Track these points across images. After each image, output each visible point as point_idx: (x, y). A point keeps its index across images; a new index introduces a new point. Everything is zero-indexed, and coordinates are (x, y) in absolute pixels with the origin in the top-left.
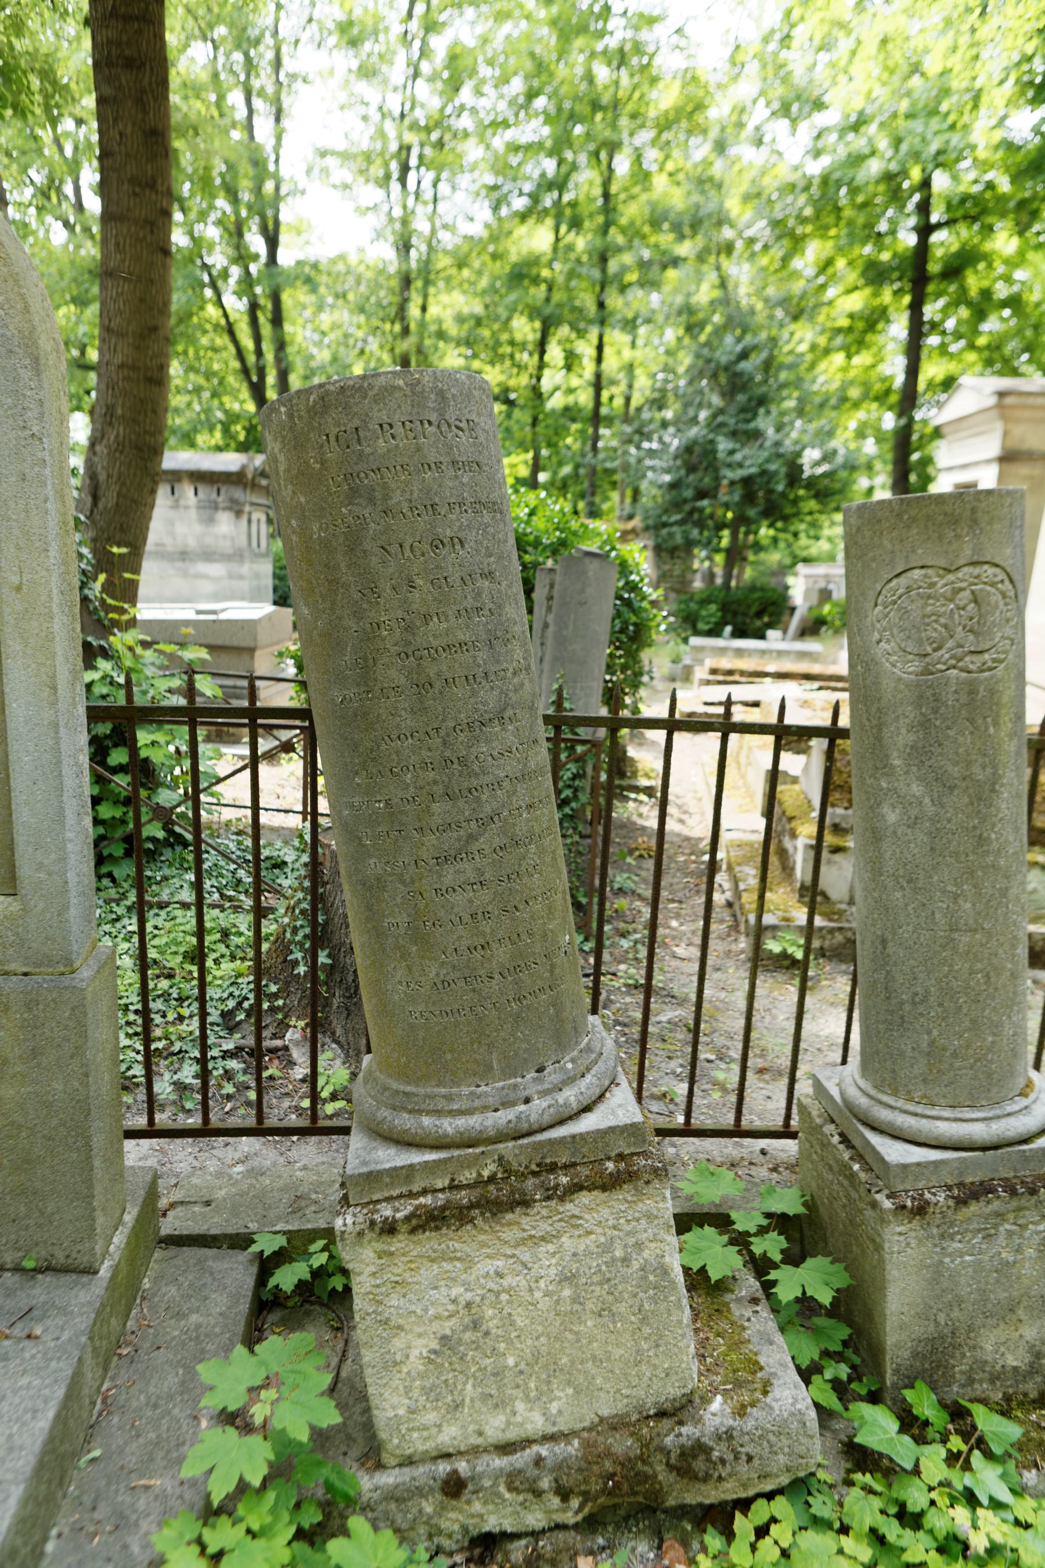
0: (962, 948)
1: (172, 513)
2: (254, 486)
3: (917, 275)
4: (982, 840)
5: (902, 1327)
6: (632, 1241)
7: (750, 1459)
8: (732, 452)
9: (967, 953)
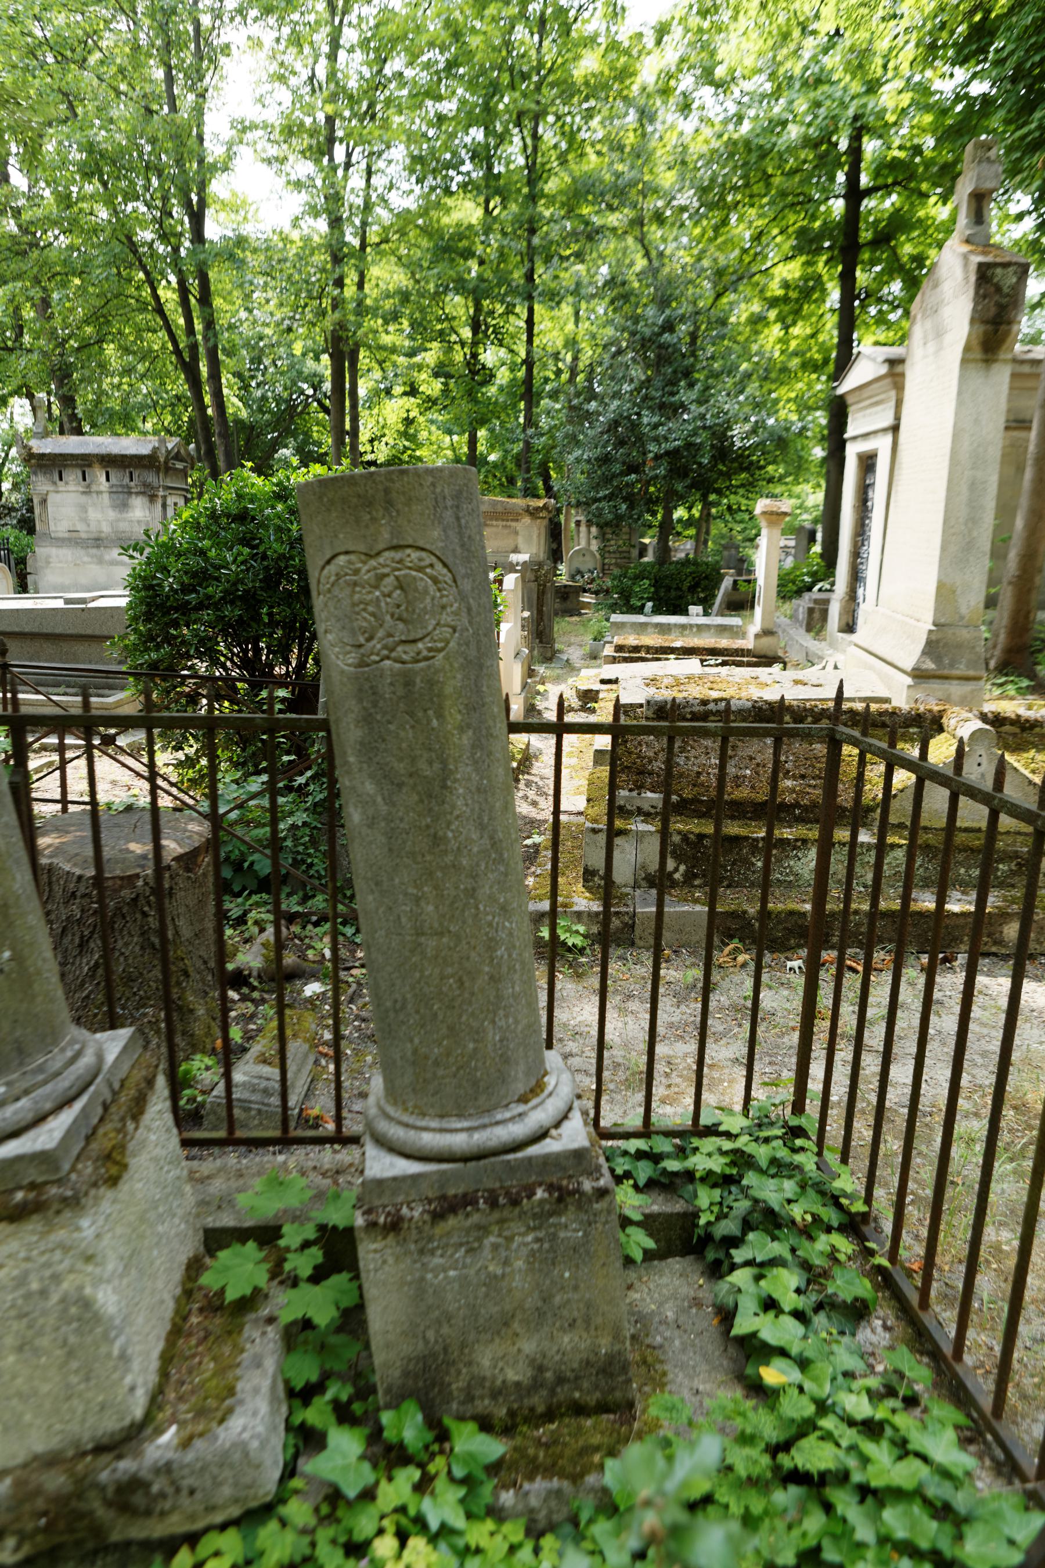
0: (430, 952)
1: (84, 499)
2: (168, 470)
3: (847, 245)
4: (437, 840)
5: (388, 1346)
6: (48, 1273)
7: (192, 1492)
8: (656, 426)
9: (436, 957)
